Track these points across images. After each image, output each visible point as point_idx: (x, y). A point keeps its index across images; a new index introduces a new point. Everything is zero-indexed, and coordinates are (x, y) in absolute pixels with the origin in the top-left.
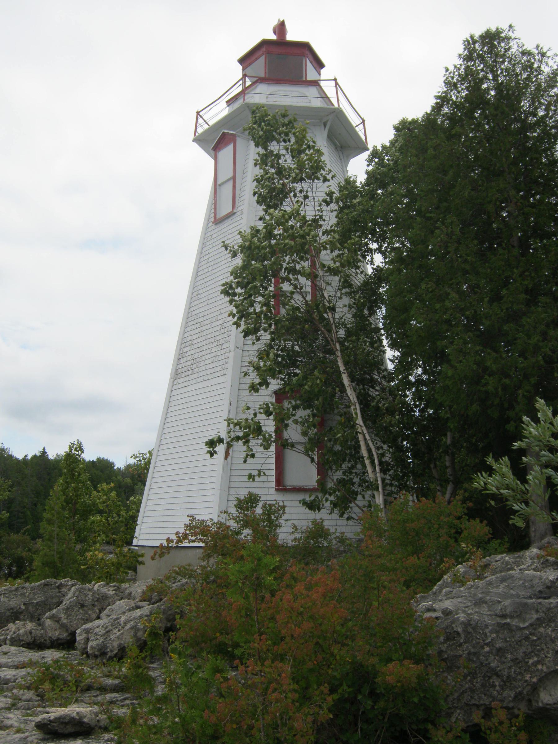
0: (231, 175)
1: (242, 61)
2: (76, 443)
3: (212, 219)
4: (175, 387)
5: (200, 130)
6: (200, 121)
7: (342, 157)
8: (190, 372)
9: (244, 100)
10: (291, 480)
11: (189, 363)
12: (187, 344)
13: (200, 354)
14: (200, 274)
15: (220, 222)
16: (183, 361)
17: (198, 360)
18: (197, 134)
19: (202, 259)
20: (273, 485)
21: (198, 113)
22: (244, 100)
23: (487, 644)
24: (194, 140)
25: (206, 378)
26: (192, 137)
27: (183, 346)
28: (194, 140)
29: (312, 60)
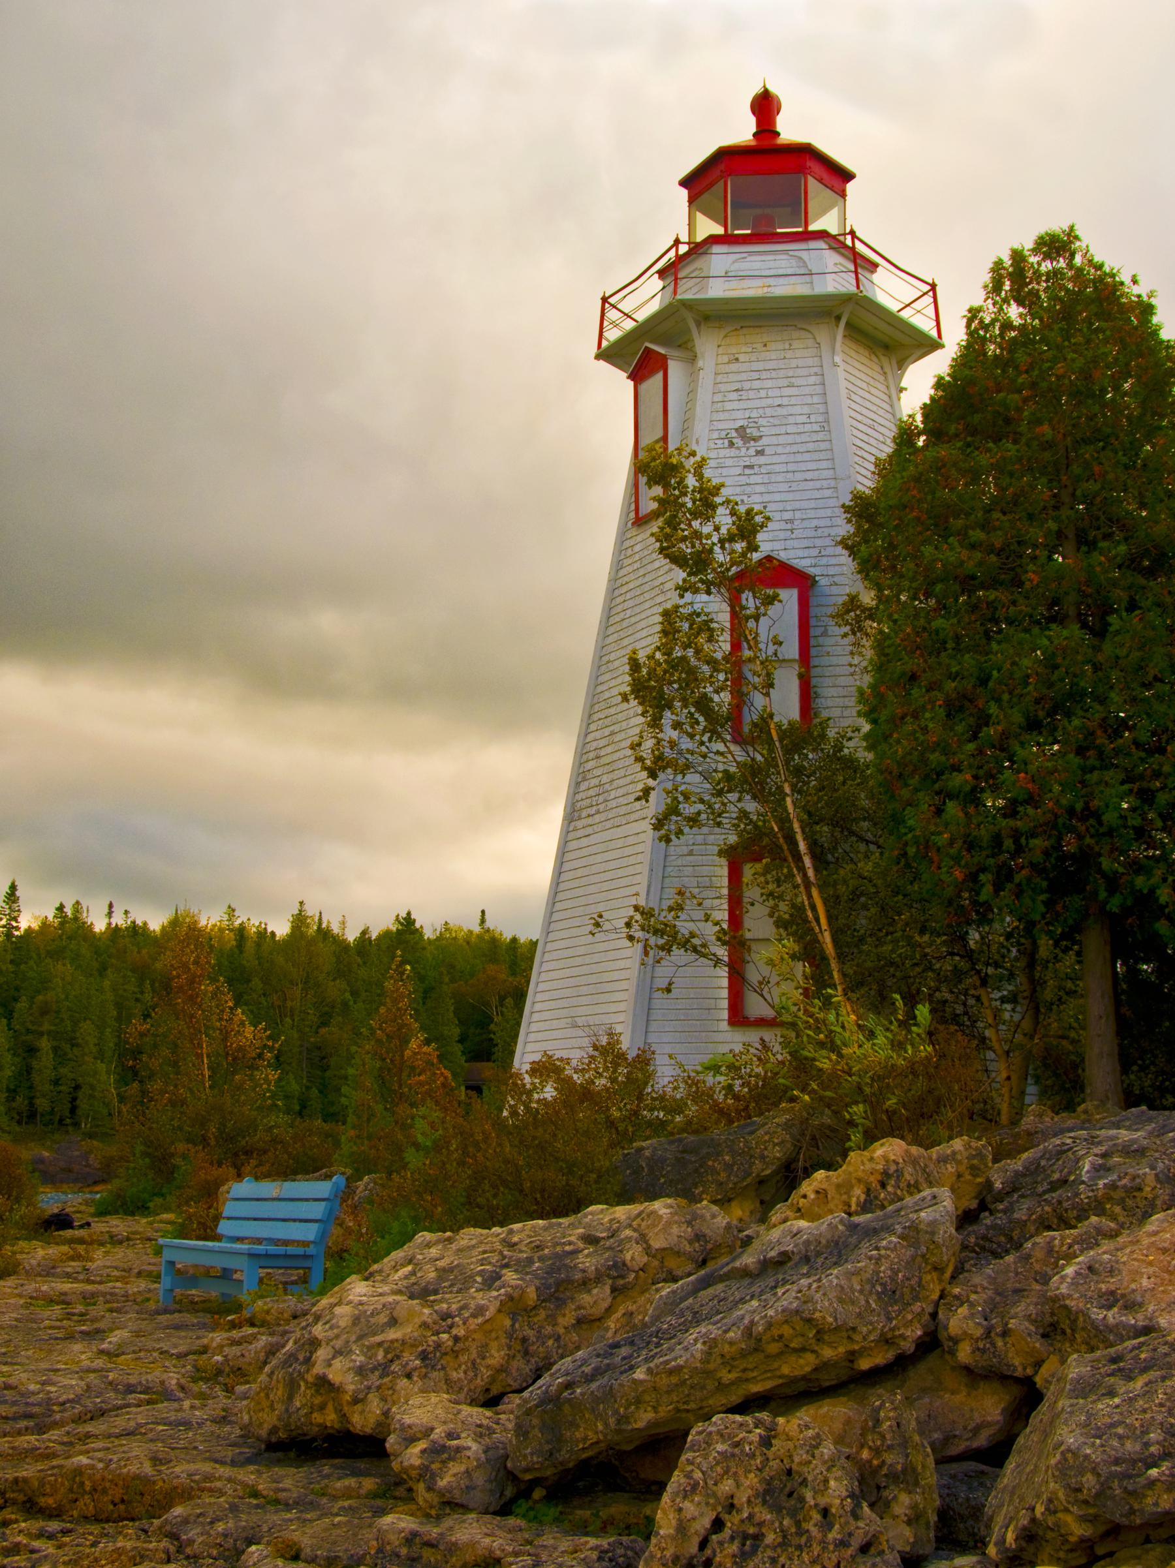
0: (660, 434)
1: (685, 183)
2: (70, 1129)
3: (632, 515)
4: (571, 836)
5: (612, 335)
6: (612, 314)
7: (887, 369)
8: (595, 808)
9: (675, 293)
10: (756, 1007)
11: (592, 792)
12: (592, 755)
13: (611, 776)
14: (612, 620)
15: (646, 523)
16: (583, 786)
17: (607, 787)
18: (605, 344)
19: (617, 593)
20: (725, 1015)
21: (605, 300)
22: (675, 293)
23: (663, 1176)
24: (598, 357)
25: (617, 821)
26: (594, 350)
27: (585, 757)
28: (598, 357)
29: (825, 176)
